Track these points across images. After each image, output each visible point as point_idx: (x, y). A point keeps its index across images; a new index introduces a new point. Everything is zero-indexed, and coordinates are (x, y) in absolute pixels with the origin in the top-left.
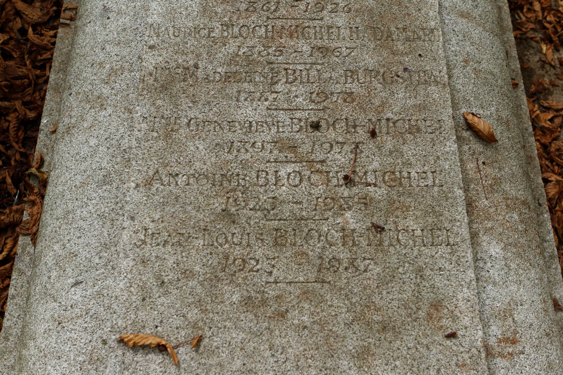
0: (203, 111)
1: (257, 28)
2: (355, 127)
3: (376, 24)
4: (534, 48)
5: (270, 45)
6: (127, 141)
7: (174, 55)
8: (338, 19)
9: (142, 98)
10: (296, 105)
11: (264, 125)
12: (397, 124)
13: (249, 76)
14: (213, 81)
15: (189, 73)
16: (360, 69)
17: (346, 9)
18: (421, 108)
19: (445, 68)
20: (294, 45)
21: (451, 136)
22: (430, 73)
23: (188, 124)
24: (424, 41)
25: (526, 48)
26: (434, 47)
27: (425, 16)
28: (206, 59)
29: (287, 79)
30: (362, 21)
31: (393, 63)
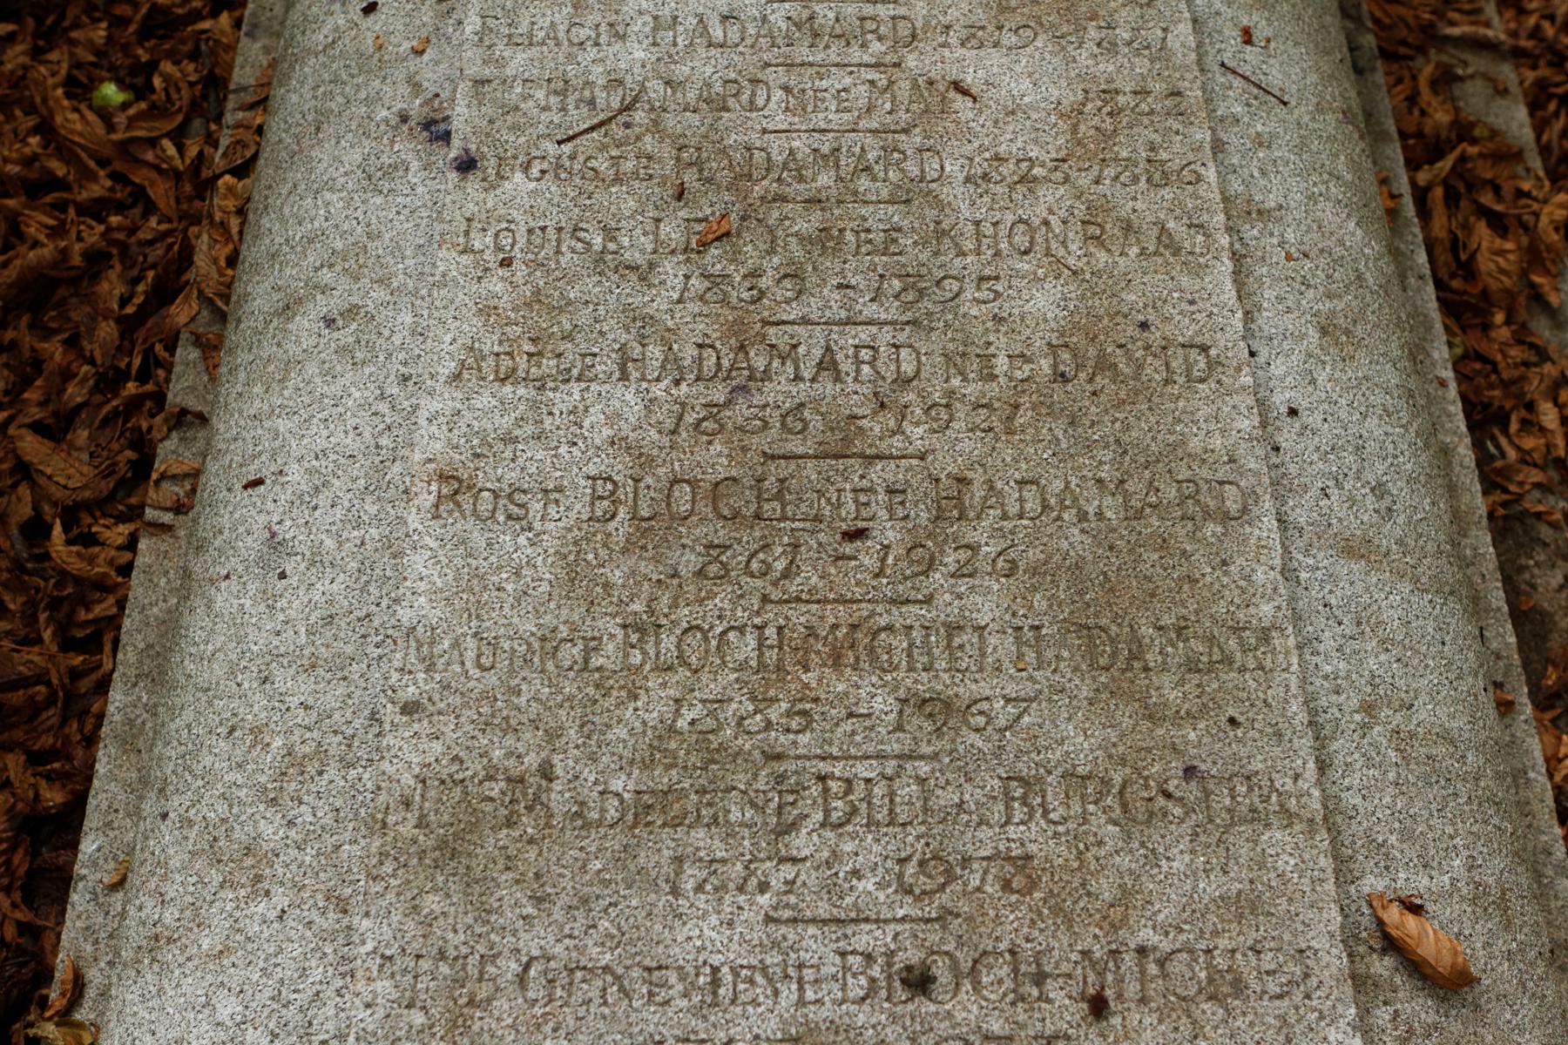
0: (567, 931)
1: (732, 636)
2: (1040, 979)
3: (1096, 616)
4: (1546, 545)
5: (772, 693)
6: (332, 1012)
7: (479, 735)
8: (979, 600)
9: (378, 887)
10: (855, 904)
11: (759, 979)
12: (1169, 967)
13: (710, 804)
14: (599, 823)
15: (525, 795)
16: (1050, 773)
17: (1000, 563)
18: (1245, 906)
19: (1311, 765)
20: (846, 694)
21: (1340, 1008)
22: (1265, 783)
23: (522, 980)
24: (1243, 670)
25: (1522, 546)
26: (1276, 692)
27: (1243, 583)
28: (577, 747)
29: (827, 813)
30: (1050, 606)
31: (1149, 750)
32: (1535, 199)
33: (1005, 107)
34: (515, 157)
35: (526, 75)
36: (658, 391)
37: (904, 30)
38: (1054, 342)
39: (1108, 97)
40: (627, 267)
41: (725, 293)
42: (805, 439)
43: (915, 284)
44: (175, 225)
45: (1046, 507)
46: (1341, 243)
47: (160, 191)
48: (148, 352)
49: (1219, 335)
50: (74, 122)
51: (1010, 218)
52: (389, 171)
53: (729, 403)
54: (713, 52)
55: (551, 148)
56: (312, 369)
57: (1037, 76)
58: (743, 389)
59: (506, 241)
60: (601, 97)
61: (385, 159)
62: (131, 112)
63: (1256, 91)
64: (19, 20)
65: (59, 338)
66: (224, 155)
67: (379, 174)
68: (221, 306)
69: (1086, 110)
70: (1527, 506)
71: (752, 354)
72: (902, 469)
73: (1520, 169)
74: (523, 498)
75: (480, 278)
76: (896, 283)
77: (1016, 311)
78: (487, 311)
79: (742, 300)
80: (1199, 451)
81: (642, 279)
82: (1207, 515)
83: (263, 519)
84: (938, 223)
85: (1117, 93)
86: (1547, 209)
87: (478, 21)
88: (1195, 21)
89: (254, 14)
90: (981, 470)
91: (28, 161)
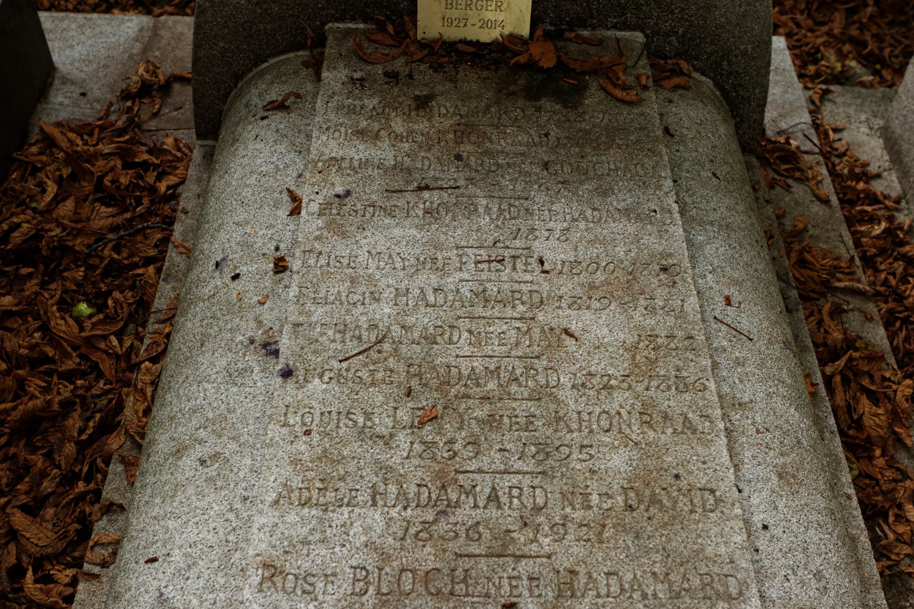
32: (894, 382)
33: (594, 344)
34: (315, 369)
35: (323, 321)
36: (394, 513)
37: (536, 299)
38: (625, 486)
39: (652, 339)
40: (378, 437)
41: (434, 453)
42: (480, 545)
43: (544, 450)
44: (114, 386)
45: (622, 590)
46: (787, 421)
47: (107, 366)
48: (93, 464)
49: (721, 483)
50: (61, 325)
51: (598, 410)
52: (242, 372)
53: (435, 521)
54: (429, 309)
55: (335, 364)
56: (191, 490)
57: (611, 326)
58: (444, 513)
59: (308, 420)
60: (365, 334)
61: (240, 365)
62: (94, 320)
63: (734, 333)
64: (35, 266)
65: (41, 452)
66: (146, 350)
67: (236, 374)
68: (139, 442)
69: (640, 346)
70: (903, 568)
71: (449, 491)
72: (537, 565)
73: (884, 366)
74: (311, 579)
75: (292, 442)
76: (533, 448)
77: (602, 467)
78: (295, 462)
79: (443, 458)
80: (712, 555)
81: (386, 444)
82: (719, 596)
83: (156, 584)
84: (556, 412)
85: (657, 336)
86: (901, 388)
87: (297, 289)
88: (699, 293)
89: (168, 269)
90: (584, 566)
91: (32, 347)
